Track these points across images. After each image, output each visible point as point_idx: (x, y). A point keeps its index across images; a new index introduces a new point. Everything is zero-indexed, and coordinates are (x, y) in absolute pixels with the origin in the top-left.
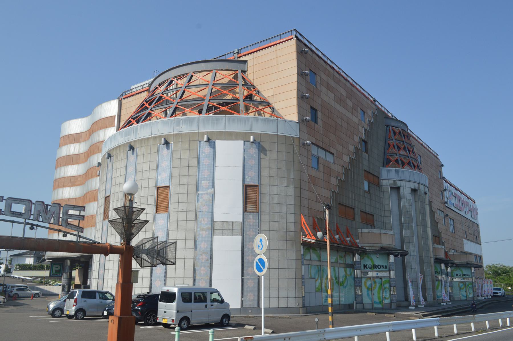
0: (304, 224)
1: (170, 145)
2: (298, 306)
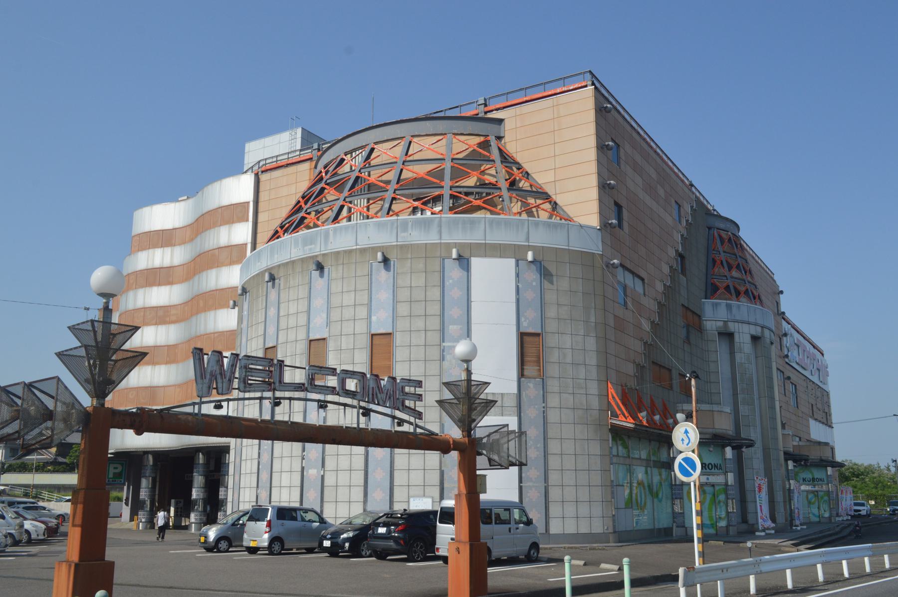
0: (613, 397)
1: (392, 262)
2: (606, 531)
